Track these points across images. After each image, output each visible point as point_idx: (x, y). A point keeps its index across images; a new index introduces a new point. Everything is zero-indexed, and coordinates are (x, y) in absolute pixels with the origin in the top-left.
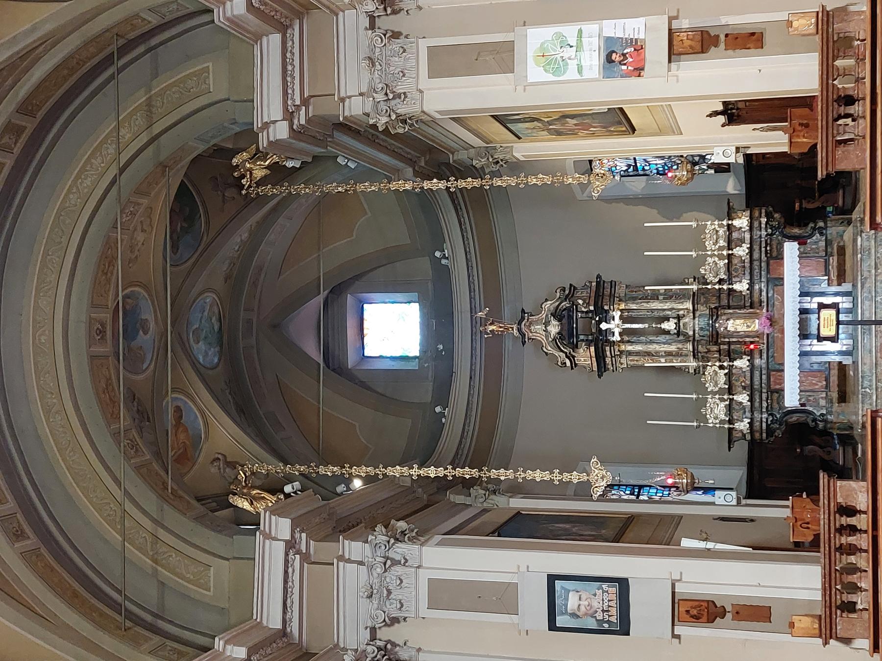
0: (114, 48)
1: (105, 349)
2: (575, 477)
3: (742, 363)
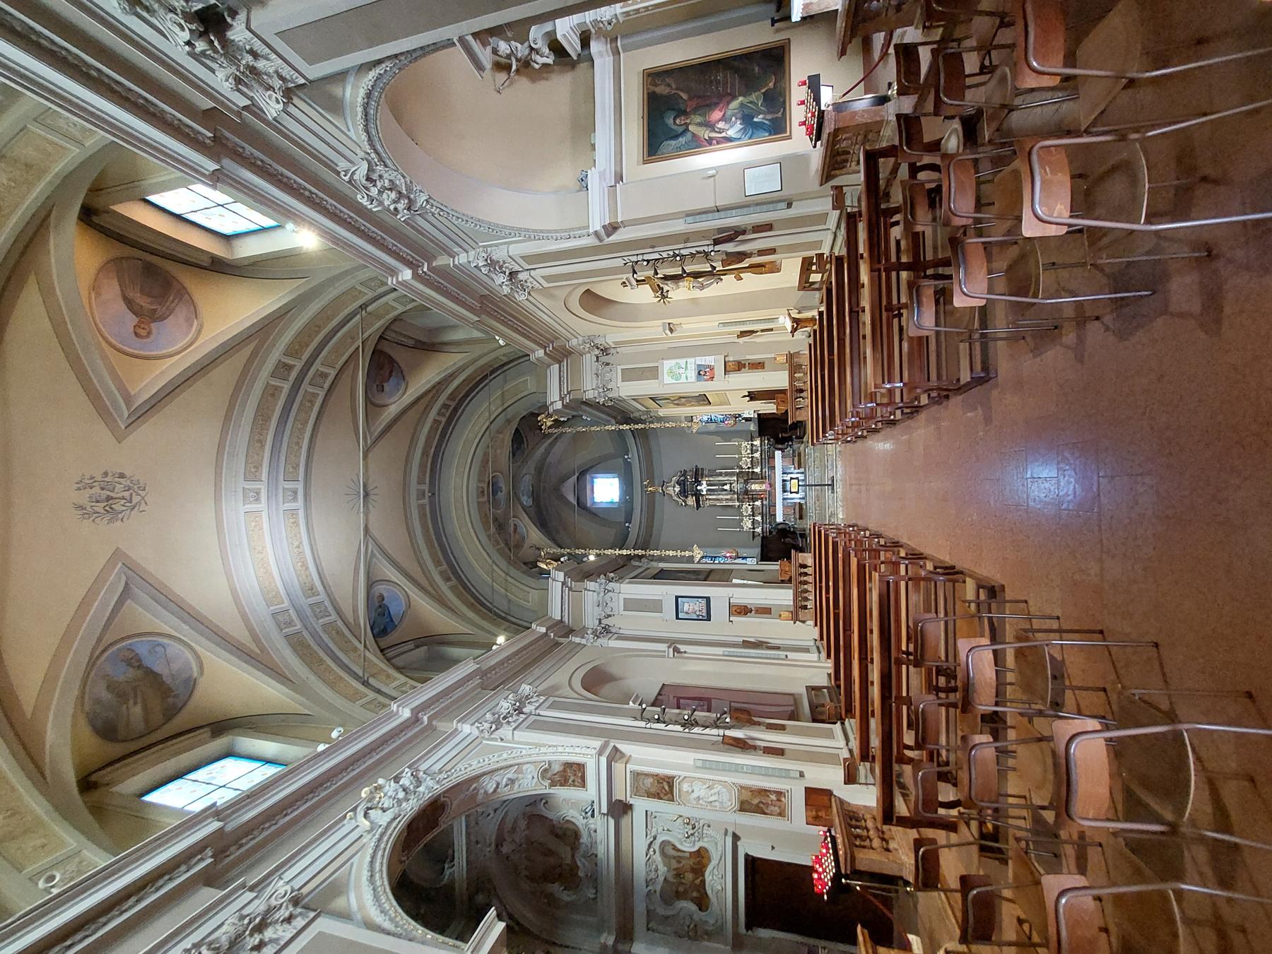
2: (687, 554)
3: (758, 503)
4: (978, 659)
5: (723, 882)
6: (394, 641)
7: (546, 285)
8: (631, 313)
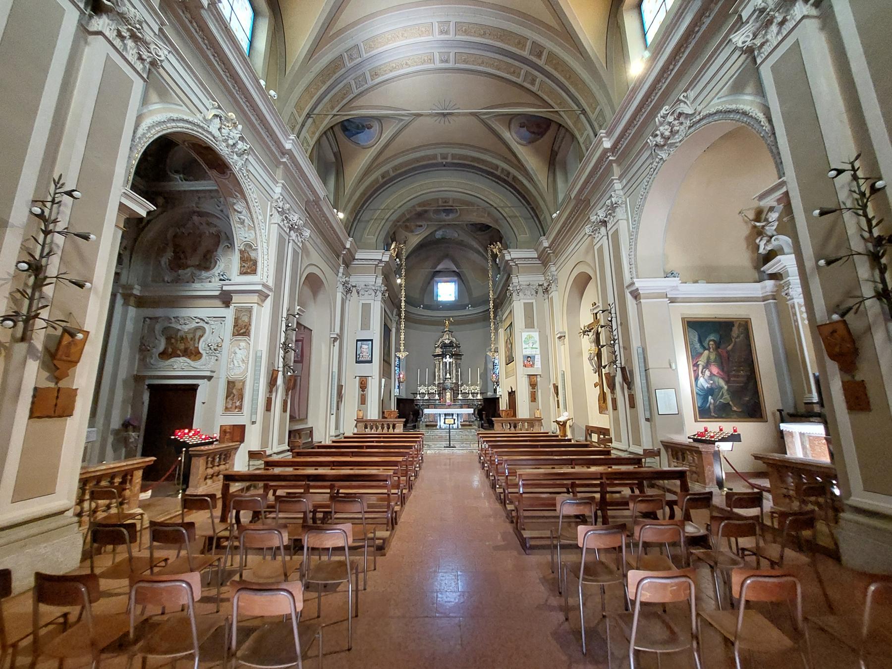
0: (533, 205)
1: (440, 203)
2: (402, 348)
3: (437, 397)
4: (337, 537)
5: (179, 369)
6: (339, 137)
7: (596, 248)
8: (573, 309)
